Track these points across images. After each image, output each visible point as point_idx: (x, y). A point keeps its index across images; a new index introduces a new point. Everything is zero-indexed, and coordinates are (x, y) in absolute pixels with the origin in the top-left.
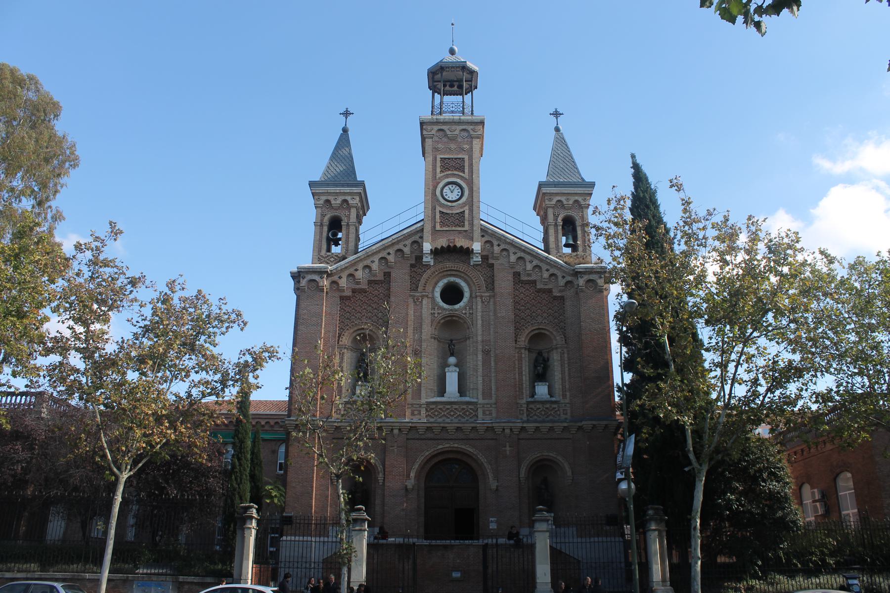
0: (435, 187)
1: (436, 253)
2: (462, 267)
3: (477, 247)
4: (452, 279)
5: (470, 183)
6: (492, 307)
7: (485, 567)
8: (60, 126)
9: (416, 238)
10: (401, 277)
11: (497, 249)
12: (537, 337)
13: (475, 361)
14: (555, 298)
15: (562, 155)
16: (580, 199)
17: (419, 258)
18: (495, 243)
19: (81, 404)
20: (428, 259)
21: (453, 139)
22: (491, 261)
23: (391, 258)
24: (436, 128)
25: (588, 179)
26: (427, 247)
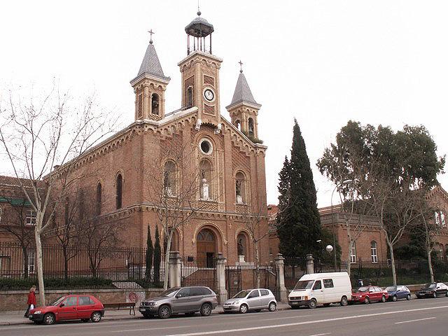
0: (217, 99)
1: (203, 125)
2: (210, 134)
3: (220, 126)
4: (206, 140)
5: (216, 92)
6: (223, 157)
7: (66, 269)
8: (363, 125)
9: (194, 115)
10: (187, 133)
11: (226, 129)
12: (239, 174)
13: (216, 182)
14: (247, 157)
15: (151, 53)
16: (162, 85)
17: (194, 126)
18: (226, 125)
19: (360, 197)
20: (198, 127)
21: (209, 66)
22: (223, 134)
23: (183, 123)
24: (203, 58)
25: (166, 75)
26: (200, 122)
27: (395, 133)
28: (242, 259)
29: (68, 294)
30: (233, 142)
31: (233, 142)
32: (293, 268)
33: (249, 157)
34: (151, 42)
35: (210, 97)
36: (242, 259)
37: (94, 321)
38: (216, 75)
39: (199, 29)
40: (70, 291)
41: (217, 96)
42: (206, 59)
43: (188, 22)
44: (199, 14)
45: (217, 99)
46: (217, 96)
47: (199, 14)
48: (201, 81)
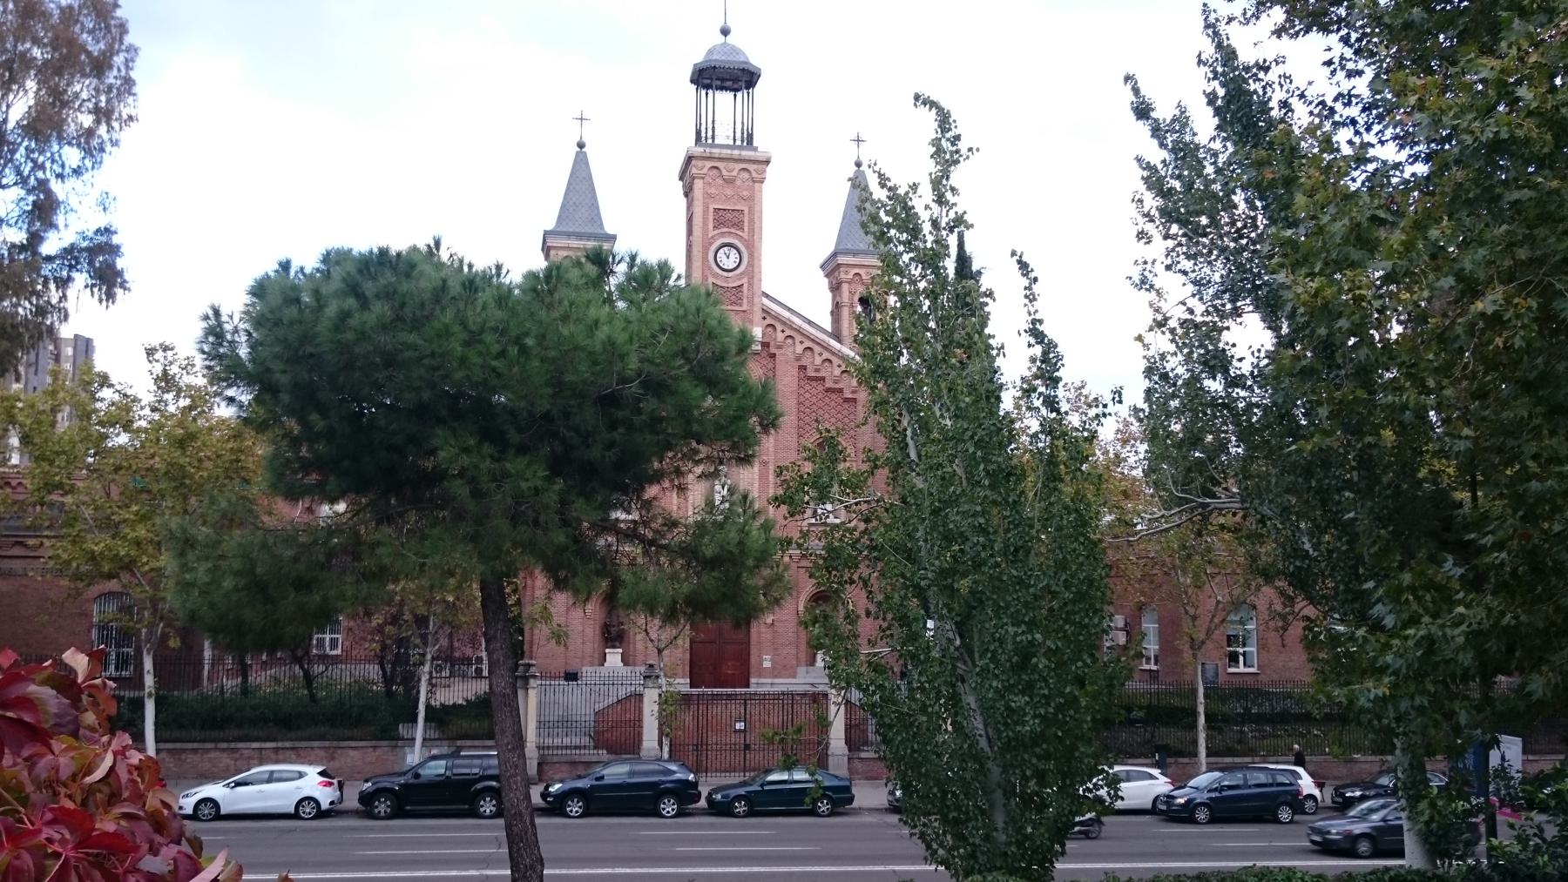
14: (846, 400)
21: (730, 182)
22: (773, 350)
24: (709, 164)
27: (1096, 313)
28: (614, 657)
29: (276, 750)
30: (803, 368)
31: (803, 368)
32: (222, 692)
33: (855, 400)
34: (581, 145)
35: (730, 263)
36: (614, 657)
37: (1277, 821)
38: (752, 200)
39: (725, 76)
40: (280, 744)
41: (751, 256)
42: (720, 165)
43: (699, 57)
44: (725, 32)
45: (751, 265)
46: (751, 256)
47: (725, 32)
48: (705, 223)
